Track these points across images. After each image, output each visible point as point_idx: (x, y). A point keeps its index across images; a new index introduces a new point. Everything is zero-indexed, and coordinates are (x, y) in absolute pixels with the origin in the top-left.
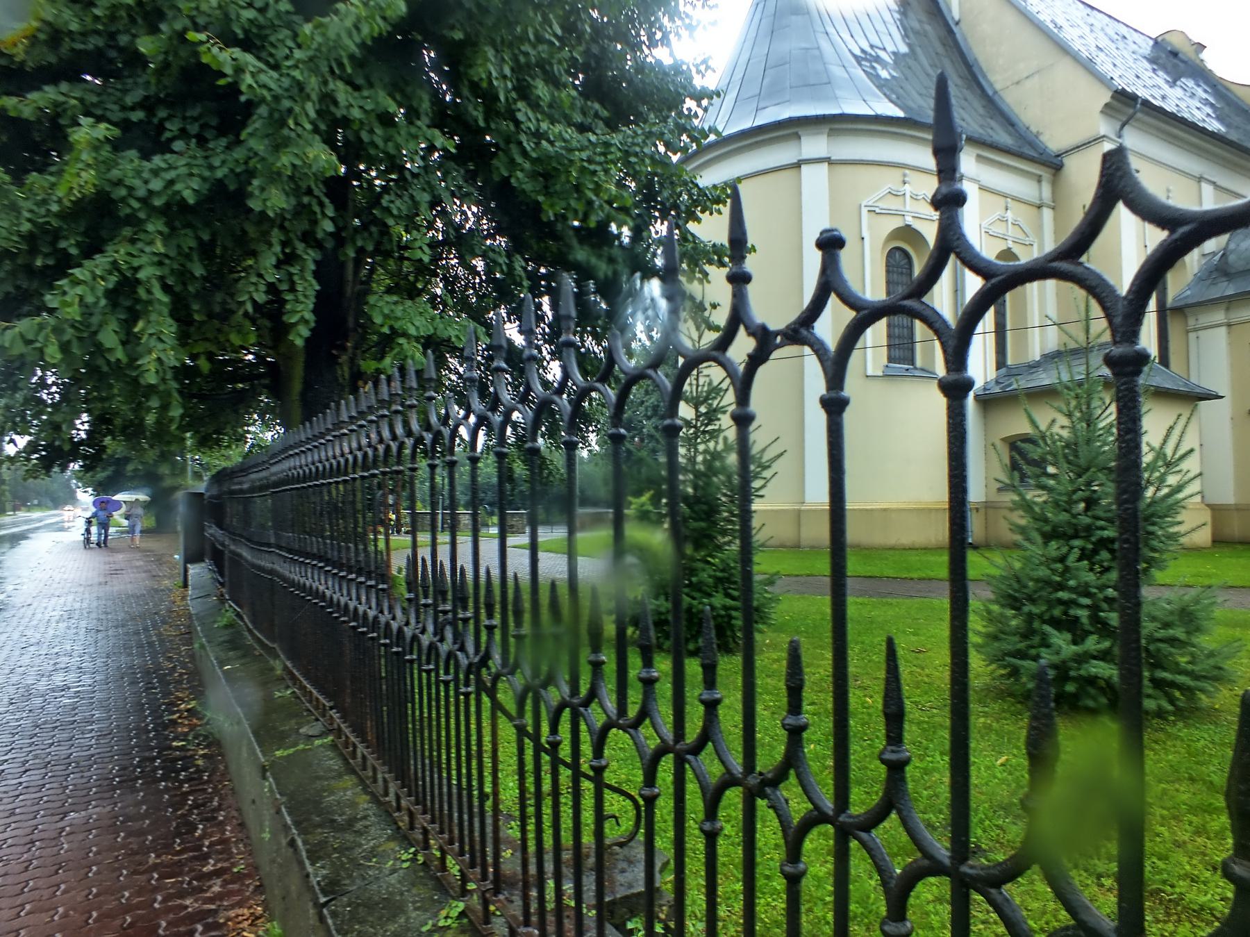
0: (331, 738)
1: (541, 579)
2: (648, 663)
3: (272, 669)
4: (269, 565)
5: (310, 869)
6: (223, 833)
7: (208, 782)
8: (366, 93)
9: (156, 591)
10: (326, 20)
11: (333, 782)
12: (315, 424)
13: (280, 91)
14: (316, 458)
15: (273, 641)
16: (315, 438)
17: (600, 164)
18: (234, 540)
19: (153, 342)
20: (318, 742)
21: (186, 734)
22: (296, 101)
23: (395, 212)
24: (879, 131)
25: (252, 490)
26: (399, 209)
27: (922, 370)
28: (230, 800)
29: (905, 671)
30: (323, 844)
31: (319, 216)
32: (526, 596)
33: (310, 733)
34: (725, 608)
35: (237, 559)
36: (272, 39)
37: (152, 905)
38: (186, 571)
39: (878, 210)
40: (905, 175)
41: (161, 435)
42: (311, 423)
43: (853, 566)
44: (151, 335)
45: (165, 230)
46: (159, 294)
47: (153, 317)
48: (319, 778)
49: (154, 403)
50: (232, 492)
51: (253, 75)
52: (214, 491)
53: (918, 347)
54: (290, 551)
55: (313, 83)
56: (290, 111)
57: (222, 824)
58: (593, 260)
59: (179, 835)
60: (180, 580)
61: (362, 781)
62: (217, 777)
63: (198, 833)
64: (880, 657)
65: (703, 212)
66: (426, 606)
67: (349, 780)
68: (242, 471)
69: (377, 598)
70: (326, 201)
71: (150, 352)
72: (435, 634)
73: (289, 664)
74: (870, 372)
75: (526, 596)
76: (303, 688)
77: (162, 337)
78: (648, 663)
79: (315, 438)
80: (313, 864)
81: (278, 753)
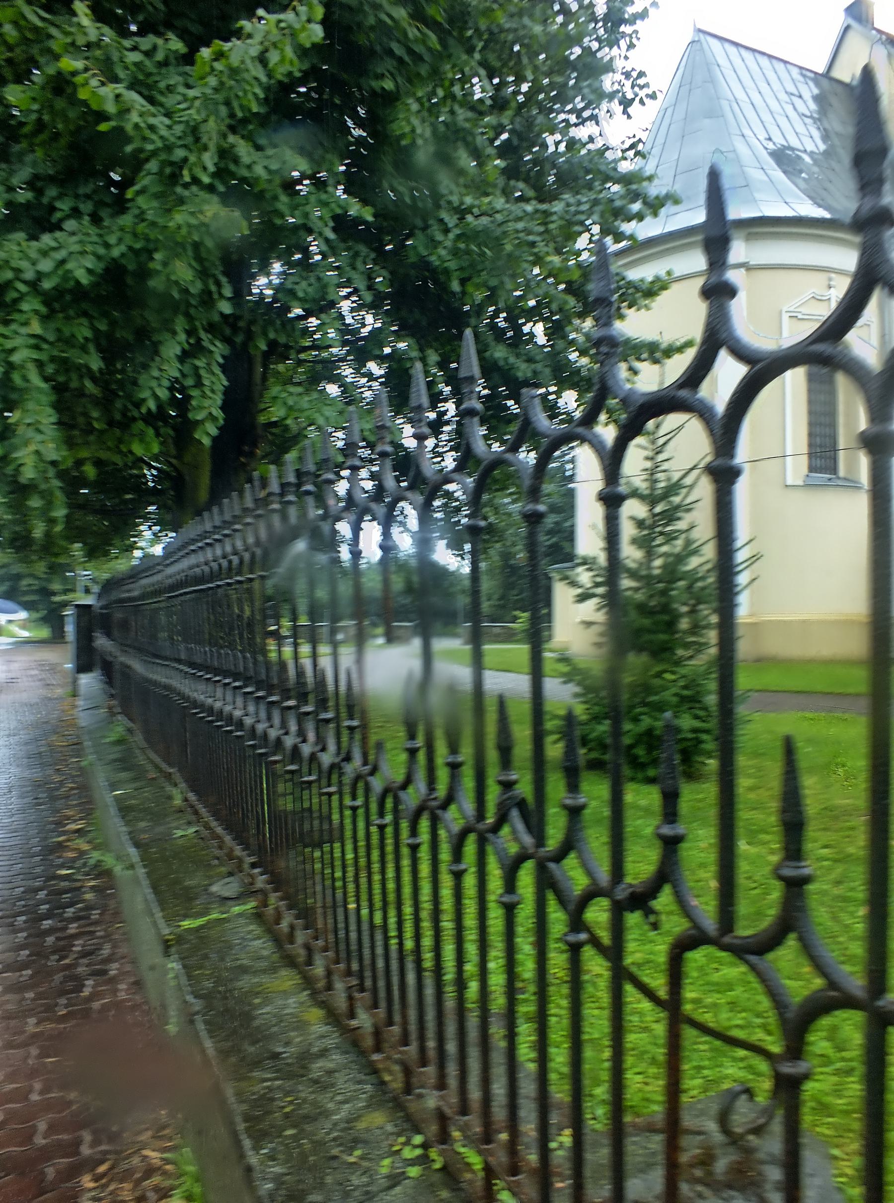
0: (253, 904)
1: (548, 707)
2: (573, 787)
3: (170, 798)
4: (164, 680)
5: (253, 1160)
6: (115, 991)
7: (96, 923)
8: (270, 152)
9: (50, 699)
10: (227, 46)
11: (264, 979)
12: (226, 509)
13: (172, 139)
14: (228, 549)
15: (170, 765)
16: (226, 524)
17: (540, 234)
18: (122, 651)
19: (30, 433)
20: (237, 909)
21: (74, 860)
22: (190, 150)
23: (301, 294)
24: (807, 235)
25: (142, 597)
26: (305, 292)
27: (845, 479)
28: (123, 950)
29: (809, 784)
30: (265, 1101)
31: (216, 296)
32: (522, 733)
33: (227, 894)
34: (695, 731)
35: (127, 672)
36: (162, 85)
37: (26, 1098)
38: (75, 681)
39: (800, 316)
40: (830, 279)
41: (49, 547)
42: (220, 505)
43: (743, 681)
44: (29, 425)
45: (43, 310)
46: (36, 380)
47: (31, 405)
48: (244, 970)
49: (35, 502)
50: (122, 601)
51: (141, 115)
52: (103, 602)
53: (841, 455)
54: (192, 665)
55: (212, 129)
56: (185, 160)
57: (113, 980)
58: (512, 360)
59: (62, 993)
60: (69, 689)
61: (308, 982)
62: (107, 917)
63: (86, 992)
64: (775, 769)
65: (630, 307)
66: (351, 729)
67: (287, 979)
68: (131, 577)
69: (317, 729)
70: (224, 280)
71: (26, 443)
72: (317, 743)
73: (192, 796)
74: (789, 482)
75: (522, 733)
76: (207, 826)
77: (41, 427)
78: (573, 787)
79: (226, 524)
80: (256, 1148)
81: (186, 924)
